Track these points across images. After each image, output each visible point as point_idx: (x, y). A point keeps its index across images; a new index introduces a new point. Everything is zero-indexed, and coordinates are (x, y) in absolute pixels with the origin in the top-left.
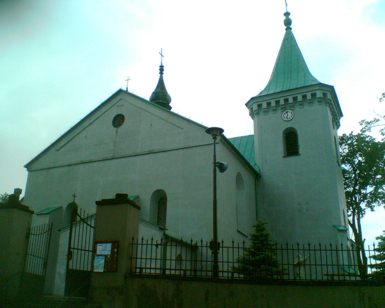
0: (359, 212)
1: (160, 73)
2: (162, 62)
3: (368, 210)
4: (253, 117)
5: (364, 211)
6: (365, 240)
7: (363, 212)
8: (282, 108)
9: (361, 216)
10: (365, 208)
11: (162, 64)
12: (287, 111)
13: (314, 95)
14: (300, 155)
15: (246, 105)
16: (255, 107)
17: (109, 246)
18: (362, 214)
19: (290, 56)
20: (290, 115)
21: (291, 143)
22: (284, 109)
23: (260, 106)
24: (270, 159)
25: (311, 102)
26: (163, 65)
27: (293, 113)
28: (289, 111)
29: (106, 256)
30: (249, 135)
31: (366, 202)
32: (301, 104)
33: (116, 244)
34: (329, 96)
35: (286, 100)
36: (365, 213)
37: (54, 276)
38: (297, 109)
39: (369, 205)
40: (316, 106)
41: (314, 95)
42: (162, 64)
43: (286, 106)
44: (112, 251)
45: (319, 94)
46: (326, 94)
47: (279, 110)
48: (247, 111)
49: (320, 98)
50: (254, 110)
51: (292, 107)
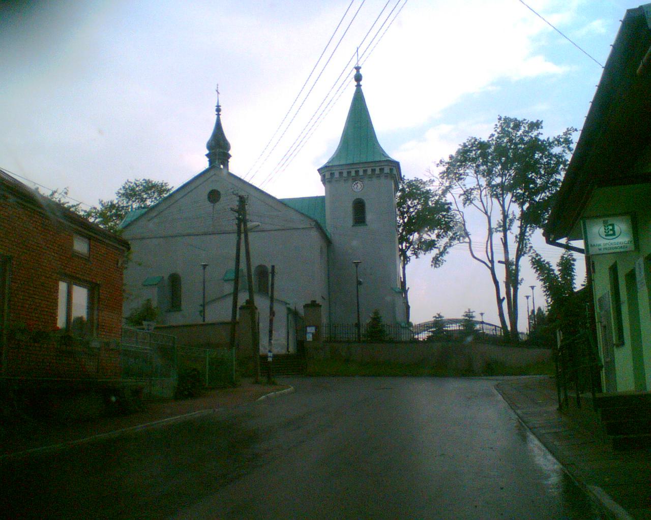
0: (406, 259)
1: (217, 114)
2: (218, 102)
3: (413, 258)
4: (324, 183)
5: (409, 259)
6: (408, 288)
7: (408, 259)
8: (353, 179)
9: (406, 262)
10: (411, 255)
11: (218, 104)
12: (356, 182)
13: (382, 170)
14: (367, 225)
15: (319, 170)
16: (328, 176)
17: (313, 328)
18: (407, 261)
19: (359, 118)
20: (359, 186)
21: (359, 208)
22: (354, 179)
23: (332, 174)
24: (339, 221)
25: (378, 176)
26: (219, 105)
27: (362, 185)
28: (359, 182)
29: (313, 333)
30: (316, 195)
31: (432, 332)
32: (370, 177)
33: (317, 327)
34: (395, 172)
35: (357, 172)
36: (409, 260)
37: (53, 315)
38: (366, 181)
39: (416, 254)
40: (383, 180)
41: (382, 170)
42: (218, 104)
43: (356, 178)
44: (316, 330)
45: (387, 170)
46: (393, 169)
47: (350, 182)
48: (318, 177)
49: (388, 173)
50: (326, 178)
51: (361, 179)
